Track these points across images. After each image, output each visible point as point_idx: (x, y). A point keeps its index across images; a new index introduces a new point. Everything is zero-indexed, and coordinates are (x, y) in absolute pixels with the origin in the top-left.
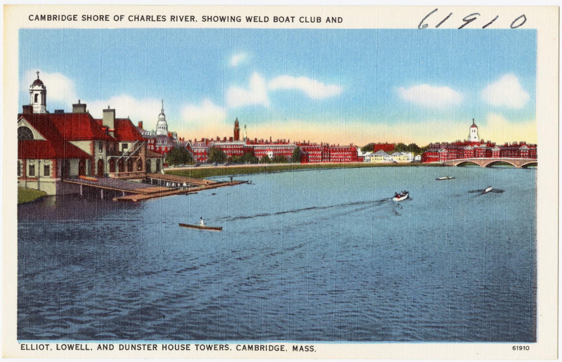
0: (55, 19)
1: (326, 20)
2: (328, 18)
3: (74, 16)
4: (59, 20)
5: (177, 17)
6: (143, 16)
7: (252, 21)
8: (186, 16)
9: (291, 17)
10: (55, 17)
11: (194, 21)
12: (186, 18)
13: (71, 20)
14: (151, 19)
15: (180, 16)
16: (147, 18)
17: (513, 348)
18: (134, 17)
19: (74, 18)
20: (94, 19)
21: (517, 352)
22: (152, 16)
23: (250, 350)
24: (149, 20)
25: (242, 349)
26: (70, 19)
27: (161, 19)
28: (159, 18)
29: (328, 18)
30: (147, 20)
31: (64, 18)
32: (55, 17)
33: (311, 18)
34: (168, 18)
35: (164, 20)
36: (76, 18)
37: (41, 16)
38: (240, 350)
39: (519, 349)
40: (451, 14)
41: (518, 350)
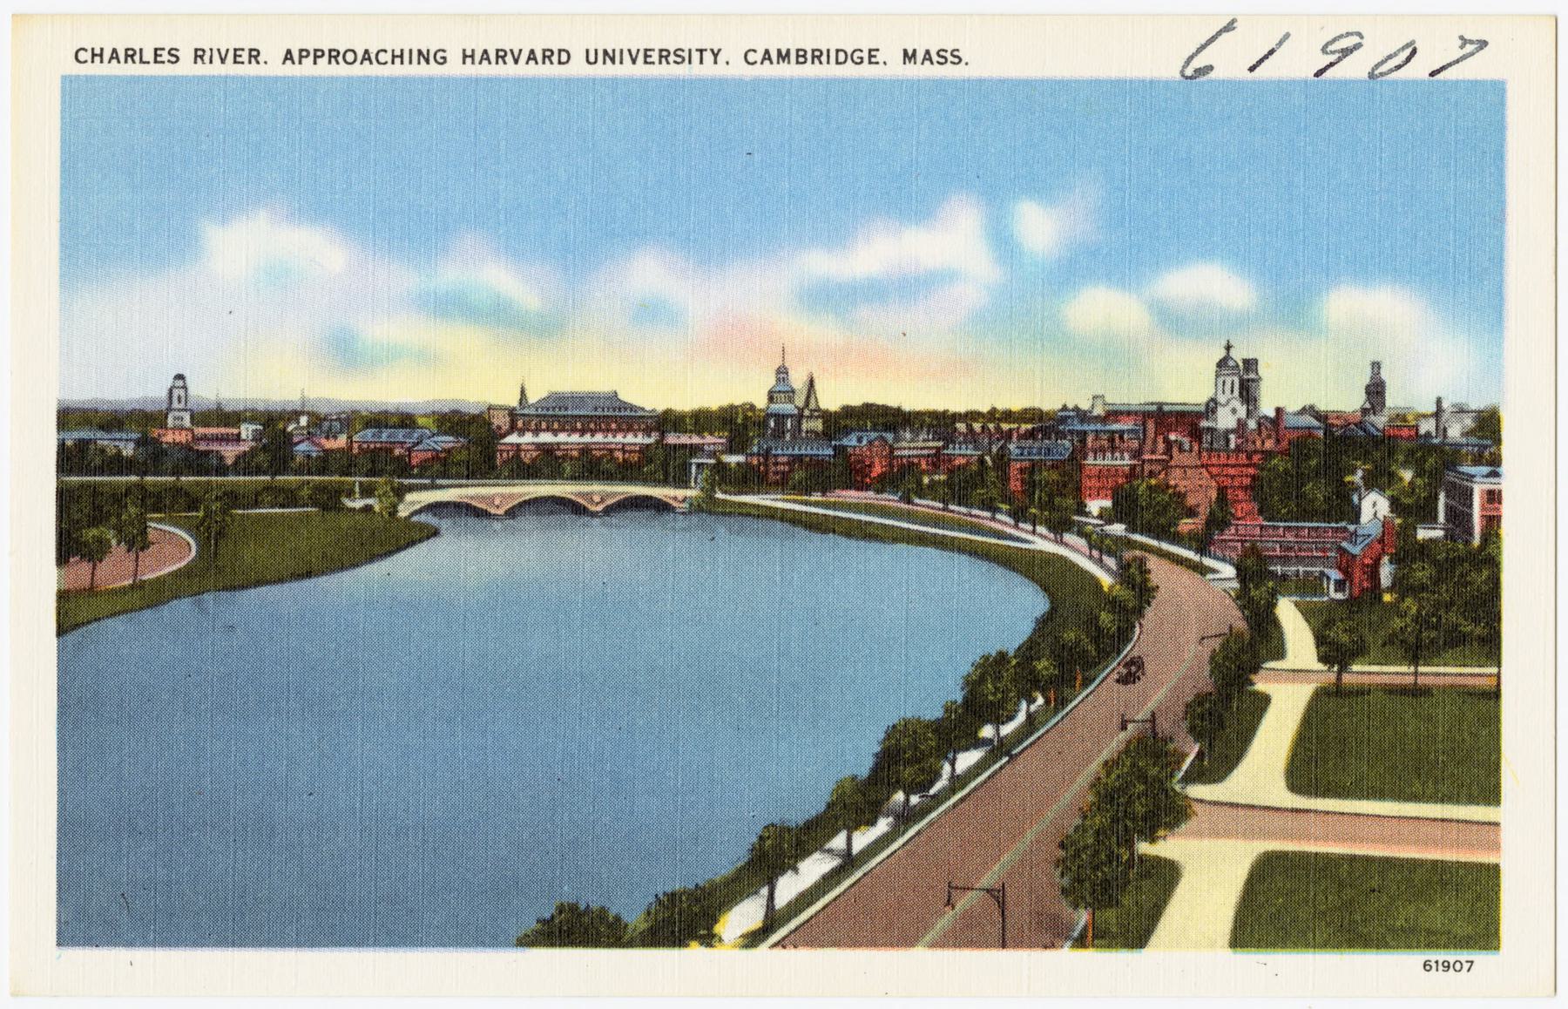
0: (547, 60)
1: (284, 57)
2: (289, 52)
3: (870, 51)
4: (828, 63)
5: (622, 51)
6: (532, 52)
7: (637, 62)
8: (646, 50)
9: (697, 50)
10: (817, 53)
11: (258, 63)
12: (646, 56)
13: (862, 62)
14: (137, 58)
15: (629, 51)
16: (127, 56)
17: (1425, 965)
18: (390, 53)
19: (870, 56)
20: (378, 61)
21: (1437, 976)
22: (141, 50)
23: (910, 62)
24: (134, 62)
25: (759, 61)
26: (442, 61)
27: (165, 56)
28: (161, 56)
29: (289, 52)
30: (126, 61)
31: (844, 56)
32: (817, 55)
33: (587, 51)
34: (186, 55)
35: (174, 59)
36: (875, 56)
37: (779, 51)
38: (756, 62)
39: (1441, 968)
40: (1287, 36)
41: (1437, 970)
